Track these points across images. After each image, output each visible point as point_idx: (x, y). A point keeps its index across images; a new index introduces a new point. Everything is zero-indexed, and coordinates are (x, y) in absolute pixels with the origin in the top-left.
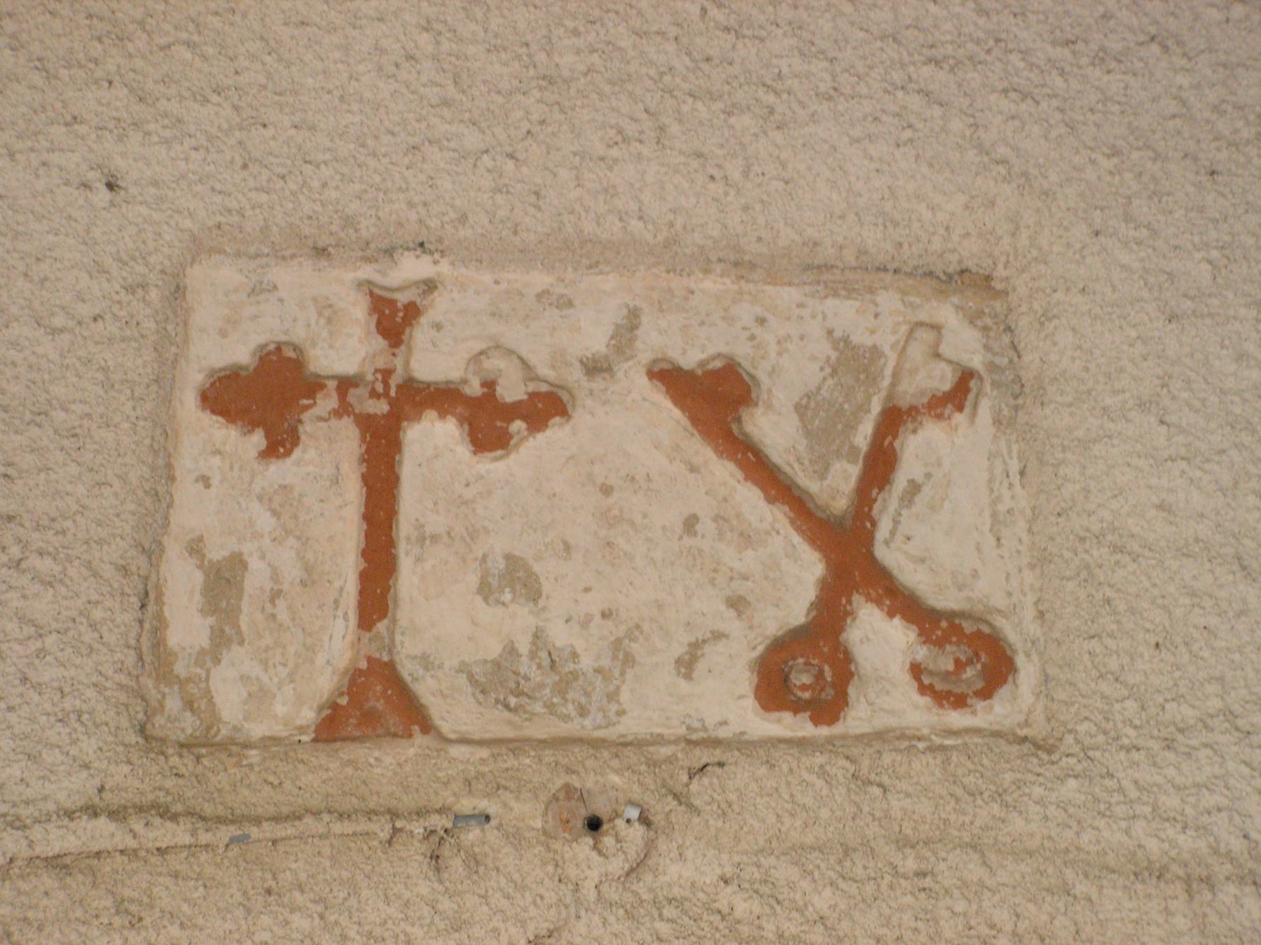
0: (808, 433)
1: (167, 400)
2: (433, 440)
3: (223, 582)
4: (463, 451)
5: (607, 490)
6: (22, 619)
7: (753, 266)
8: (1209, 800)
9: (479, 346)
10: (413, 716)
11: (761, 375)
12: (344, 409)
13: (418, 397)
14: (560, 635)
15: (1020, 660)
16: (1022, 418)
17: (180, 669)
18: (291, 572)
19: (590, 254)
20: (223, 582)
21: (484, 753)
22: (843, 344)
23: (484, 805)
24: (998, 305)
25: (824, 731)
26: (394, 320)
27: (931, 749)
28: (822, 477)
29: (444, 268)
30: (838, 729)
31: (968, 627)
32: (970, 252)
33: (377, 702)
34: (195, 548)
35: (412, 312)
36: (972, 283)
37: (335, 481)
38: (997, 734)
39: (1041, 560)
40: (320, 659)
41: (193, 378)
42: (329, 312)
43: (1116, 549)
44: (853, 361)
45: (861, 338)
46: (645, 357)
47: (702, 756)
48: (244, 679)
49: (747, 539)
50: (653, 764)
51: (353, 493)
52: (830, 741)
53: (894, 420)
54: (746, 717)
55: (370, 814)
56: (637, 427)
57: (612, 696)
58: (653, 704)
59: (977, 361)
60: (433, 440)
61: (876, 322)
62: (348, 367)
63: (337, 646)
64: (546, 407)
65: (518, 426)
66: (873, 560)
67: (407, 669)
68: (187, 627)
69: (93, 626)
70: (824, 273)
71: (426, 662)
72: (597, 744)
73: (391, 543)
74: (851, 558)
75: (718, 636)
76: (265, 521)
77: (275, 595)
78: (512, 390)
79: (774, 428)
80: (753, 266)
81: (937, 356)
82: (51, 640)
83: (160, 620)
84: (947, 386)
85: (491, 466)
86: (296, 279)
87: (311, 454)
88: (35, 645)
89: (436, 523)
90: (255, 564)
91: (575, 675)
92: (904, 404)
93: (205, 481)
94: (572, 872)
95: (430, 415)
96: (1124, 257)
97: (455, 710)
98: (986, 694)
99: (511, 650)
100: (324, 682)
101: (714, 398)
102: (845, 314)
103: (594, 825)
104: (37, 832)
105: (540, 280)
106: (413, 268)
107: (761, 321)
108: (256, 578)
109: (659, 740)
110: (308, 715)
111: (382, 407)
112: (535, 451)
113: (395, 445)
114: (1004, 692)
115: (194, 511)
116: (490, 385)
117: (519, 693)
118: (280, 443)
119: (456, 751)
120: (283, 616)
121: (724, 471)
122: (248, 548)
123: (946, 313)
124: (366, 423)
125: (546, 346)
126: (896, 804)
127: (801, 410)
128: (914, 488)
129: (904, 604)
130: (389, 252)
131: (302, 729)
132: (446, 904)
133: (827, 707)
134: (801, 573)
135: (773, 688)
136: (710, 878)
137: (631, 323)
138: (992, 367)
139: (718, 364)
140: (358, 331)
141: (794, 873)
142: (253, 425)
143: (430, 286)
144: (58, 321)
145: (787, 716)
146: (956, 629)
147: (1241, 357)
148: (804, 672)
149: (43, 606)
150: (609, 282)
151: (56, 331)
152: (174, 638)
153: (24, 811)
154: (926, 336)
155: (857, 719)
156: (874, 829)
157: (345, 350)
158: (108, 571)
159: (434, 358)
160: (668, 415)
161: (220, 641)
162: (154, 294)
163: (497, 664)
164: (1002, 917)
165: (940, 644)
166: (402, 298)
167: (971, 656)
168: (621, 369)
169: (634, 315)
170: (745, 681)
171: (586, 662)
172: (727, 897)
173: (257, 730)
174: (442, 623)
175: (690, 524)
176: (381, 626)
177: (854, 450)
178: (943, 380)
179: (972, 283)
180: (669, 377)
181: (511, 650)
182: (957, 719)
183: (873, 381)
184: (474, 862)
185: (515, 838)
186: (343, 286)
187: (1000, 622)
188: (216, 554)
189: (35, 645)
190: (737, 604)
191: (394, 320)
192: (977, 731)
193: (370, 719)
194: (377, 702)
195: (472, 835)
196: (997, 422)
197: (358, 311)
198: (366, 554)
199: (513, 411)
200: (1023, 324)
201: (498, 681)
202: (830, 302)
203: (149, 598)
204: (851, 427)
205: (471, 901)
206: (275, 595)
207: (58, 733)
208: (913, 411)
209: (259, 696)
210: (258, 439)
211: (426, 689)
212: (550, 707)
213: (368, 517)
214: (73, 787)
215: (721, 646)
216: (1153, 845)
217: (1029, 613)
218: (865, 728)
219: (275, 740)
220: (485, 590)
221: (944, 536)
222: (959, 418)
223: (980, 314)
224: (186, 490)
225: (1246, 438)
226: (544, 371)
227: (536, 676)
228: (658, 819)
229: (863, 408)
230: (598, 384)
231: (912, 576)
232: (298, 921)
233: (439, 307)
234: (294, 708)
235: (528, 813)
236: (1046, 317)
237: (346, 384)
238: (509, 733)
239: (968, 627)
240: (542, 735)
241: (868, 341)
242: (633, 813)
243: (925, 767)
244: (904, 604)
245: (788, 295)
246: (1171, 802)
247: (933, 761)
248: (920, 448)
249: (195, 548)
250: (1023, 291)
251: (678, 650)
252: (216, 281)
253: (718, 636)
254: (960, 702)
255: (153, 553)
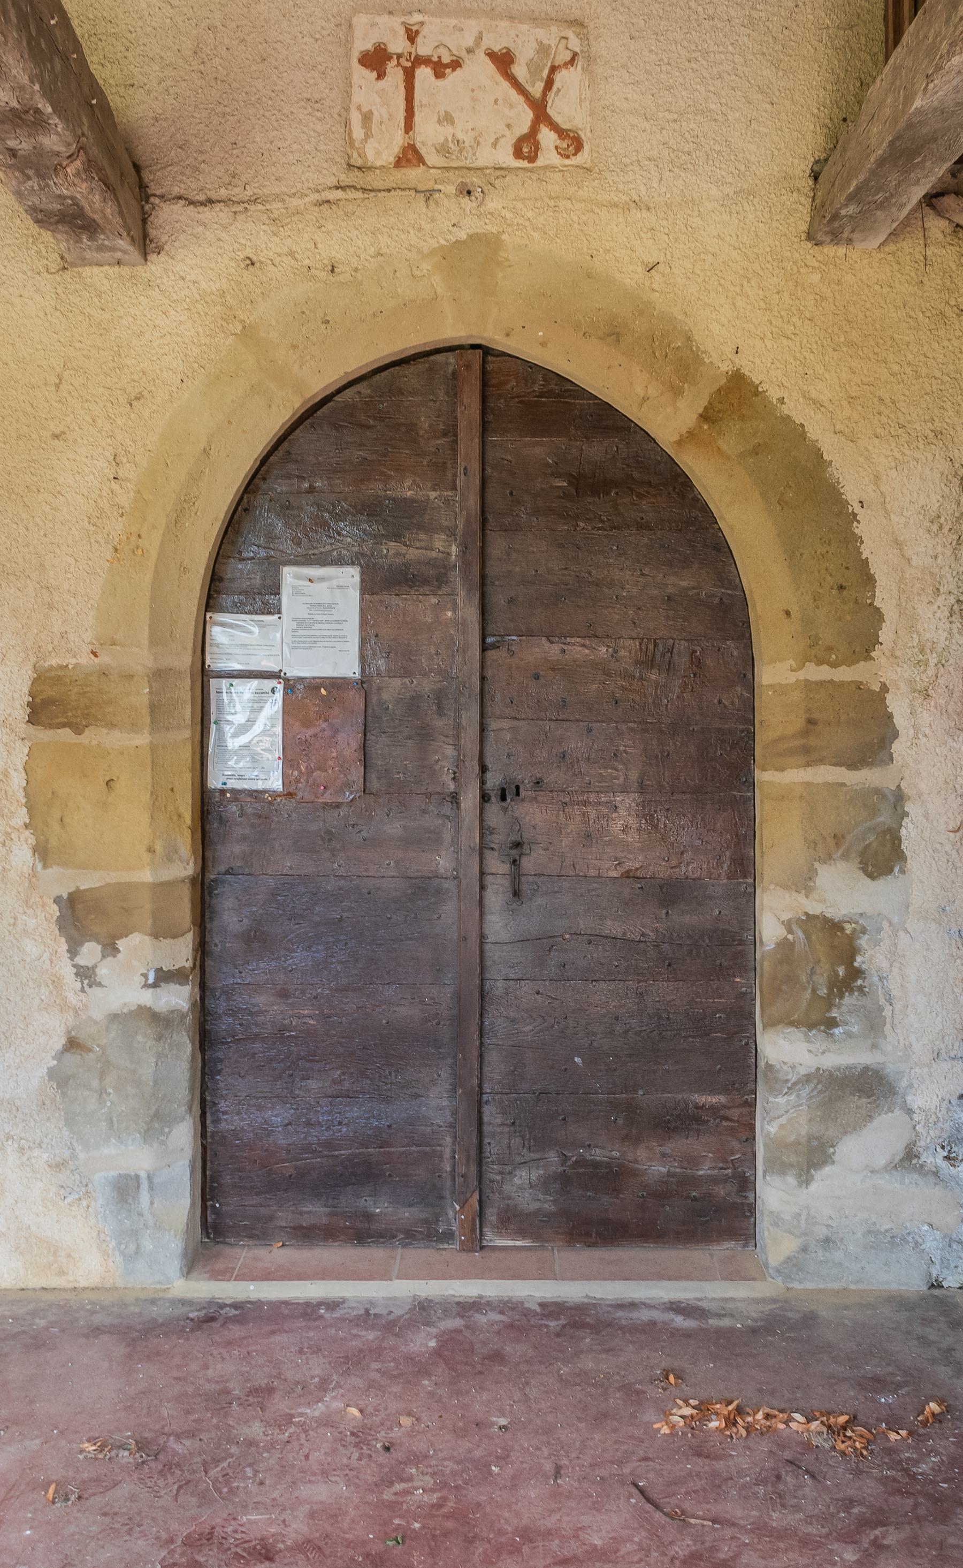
0: (530, 72)
1: (349, 62)
2: (424, 74)
3: (367, 118)
4: (433, 78)
5: (473, 90)
6: (314, 131)
7: (515, 18)
8: (631, 186)
9: (436, 44)
10: (421, 160)
11: (517, 54)
12: (399, 64)
13: (420, 61)
14: (460, 136)
15: (585, 144)
16: (590, 68)
17: (357, 145)
18: (386, 116)
19: (470, 14)
20: (367, 118)
21: (440, 171)
22: (540, 43)
23: (439, 187)
24: (585, 31)
25: (531, 165)
26: (412, 36)
27: (560, 171)
28: (533, 87)
29: (426, 18)
30: (535, 165)
31: (571, 135)
32: (577, 14)
33: (410, 156)
34: (359, 108)
35: (417, 32)
36: (577, 24)
37: (397, 87)
38: (577, 166)
39: (592, 114)
40: (395, 142)
41: (356, 55)
42: (394, 33)
43: (613, 111)
44: (543, 49)
45: (545, 42)
46: (484, 48)
47: (498, 173)
48: (374, 148)
49: (511, 106)
50: (485, 175)
51: (402, 91)
52: (533, 168)
53: (553, 69)
54: (510, 161)
55: (409, 189)
56: (480, 70)
57: (474, 154)
58: (486, 157)
59: (577, 50)
60: (424, 74)
61: (550, 35)
62: (399, 51)
63: (398, 139)
64: (456, 64)
65: (448, 71)
66: (546, 111)
67: (418, 146)
68: (358, 133)
69: (333, 133)
70: (536, 20)
71: (423, 143)
72: (469, 169)
73: (413, 107)
74: (541, 115)
75: (503, 136)
76: (378, 100)
77: (381, 123)
78: (446, 59)
79: (520, 71)
80: (515, 18)
81: (567, 48)
82: (322, 137)
83: (350, 129)
84: (569, 59)
85: (440, 83)
86: (384, 20)
87: (390, 79)
88: (318, 139)
89: (425, 101)
90: (375, 113)
91: (464, 148)
92: (557, 64)
93: (361, 87)
94: (463, 206)
95: (423, 66)
96: (620, 18)
97: (431, 158)
98: (575, 154)
99: (446, 140)
100: (396, 150)
101: (503, 61)
102: (541, 33)
103: (469, 192)
104: (323, 194)
105: (453, 22)
106: (417, 18)
107: (517, 36)
108: (376, 118)
109: (487, 168)
110: (392, 159)
111: (409, 64)
112: (453, 77)
113: (413, 77)
114: (580, 154)
115: (358, 97)
116: (440, 57)
117: (449, 153)
118: (381, 75)
119: (432, 171)
120: (384, 129)
121: (505, 85)
122: (373, 108)
123: (570, 34)
124: (405, 69)
125: (459, 42)
126: (550, 187)
127: (528, 65)
128: (559, 90)
129: (554, 127)
130: (410, 13)
131: (390, 163)
132: (430, 215)
133: (532, 159)
134: (527, 116)
135: (518, 154)
136: (500, 207)
137: (480, 37)
138: (582, 51)
139: (504, 51)
140: (401, 39)
141: (522, 206)
142: (374, 70)
143: (422, 23)
144: (317, 36)
145: (521, 161)
146: (568, 135)
147: (651, 51)
148: (526, 148)
149: (318, 127)
150: (473, 22)
151: (317, 40)
152: (354, 136)
153: (319, 187)
154: (564, 41)
155: (540, 162)
156: (543, 194)
157: (398, 45)
158: (336, 116)
159: (424, 48)
160: (490, 67)
161: (367, 136)
162: (343, 27)
163: (443, 145)
164: (575, 218)
165: (563, 139)
166: (414, 28)
167: (573, 142)
168: (477, 51)
169: (481, 33)
170: (511, 150)
171: (467, 144)
172: (504, 212)
173: (378, 164)
174: (428, 132)
175: (496, 101)
176: (411, 133)
177: (542, 78)
178: (568, 56)
179: (577, 24)
180: (491, 55)
181: (446, 140)
182: (567, 162)
183: (548, 55)
184: (437, 203)
185: (447, 196)
186: (396, 23)
187: (580, 132)
188: (364, 110)
189: (318, 139)
190: (509, 126)
191: (412, 36)
192: (572, 166)
193: (408, 161)
194: (410, 156)
195: (437, 195)
196: (583, 69)
197: (402, 31)
198: (406, 111)
199: (446, 66)
200: (591, 38)
201: (442, 149)
202: (538, 30)
203: (347, 124)
204: (542, 71)
205: (436, 214)
206: (381, 123)
207: (325, 165)
208: (559, 66)
209: (378, 153)
210: (375, 74)
211: (423, 151)
212: (457, 157)
213: (406, 99)
214: (332, 181)
215: (504, 139)
216: (616, 199)
217: (588, 130)
218: (542, 165)
219: (384, 167)
220: (439, 122)
221: (562, 108)
222: (572, 69)
223: (580, 34)
224: (355, 90)
225: (650, 77)
226: (455, 52)
227: (453, 148)
228: (486, 191)
229: (546, 64)
230: (471, 56)
231: (557, 118)
232: (392, 219)
233: (424, 31)
234: (388, 157)
235: (452, 189)
236: (599, 36)
237: (399, 56)
238: (446, 165)
239: (571, 135)
240: (455, 166)
241: (548, 42)
242: (480, 190)
243: (558, 176)
244: (554, 127)
245: (525, 27)
246: (621, 186)
247: (560, 174)
248: (559, 77)
249: (359, 108)
250: (592, 27)
251: (493, 140)
252: (361, 21)
253: (503, 136)
254: (568, 157)
255: (347, 110)
